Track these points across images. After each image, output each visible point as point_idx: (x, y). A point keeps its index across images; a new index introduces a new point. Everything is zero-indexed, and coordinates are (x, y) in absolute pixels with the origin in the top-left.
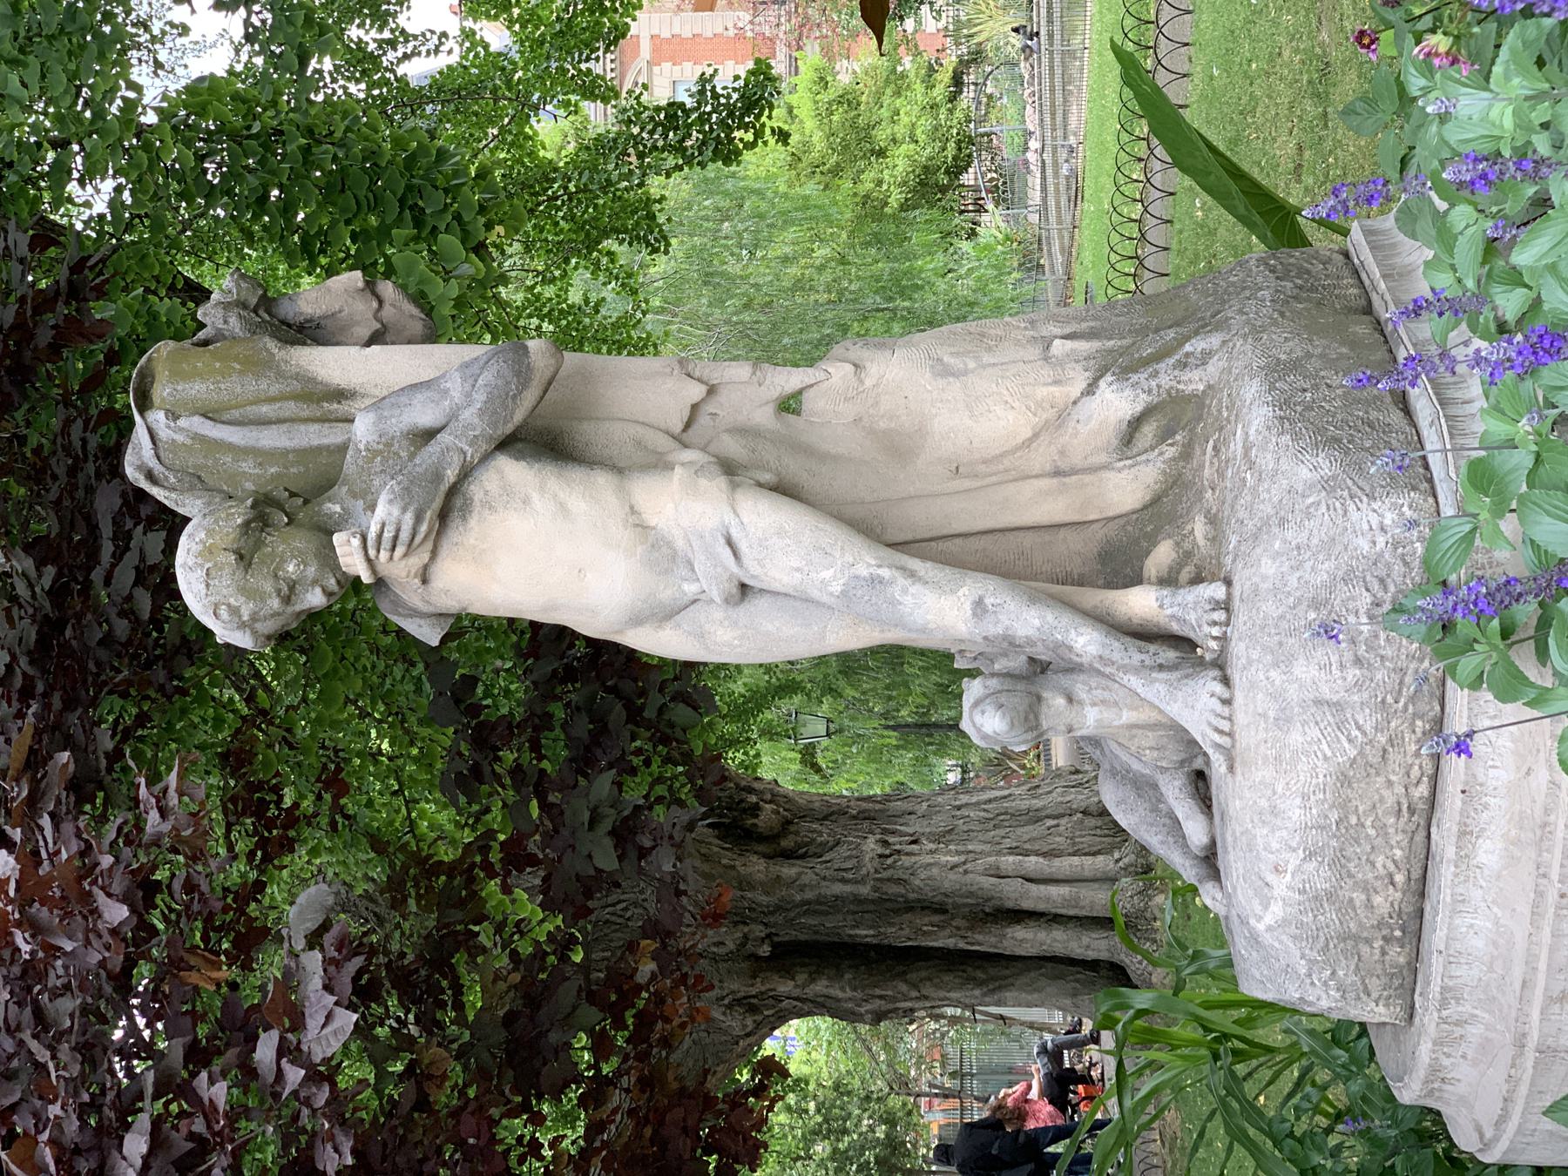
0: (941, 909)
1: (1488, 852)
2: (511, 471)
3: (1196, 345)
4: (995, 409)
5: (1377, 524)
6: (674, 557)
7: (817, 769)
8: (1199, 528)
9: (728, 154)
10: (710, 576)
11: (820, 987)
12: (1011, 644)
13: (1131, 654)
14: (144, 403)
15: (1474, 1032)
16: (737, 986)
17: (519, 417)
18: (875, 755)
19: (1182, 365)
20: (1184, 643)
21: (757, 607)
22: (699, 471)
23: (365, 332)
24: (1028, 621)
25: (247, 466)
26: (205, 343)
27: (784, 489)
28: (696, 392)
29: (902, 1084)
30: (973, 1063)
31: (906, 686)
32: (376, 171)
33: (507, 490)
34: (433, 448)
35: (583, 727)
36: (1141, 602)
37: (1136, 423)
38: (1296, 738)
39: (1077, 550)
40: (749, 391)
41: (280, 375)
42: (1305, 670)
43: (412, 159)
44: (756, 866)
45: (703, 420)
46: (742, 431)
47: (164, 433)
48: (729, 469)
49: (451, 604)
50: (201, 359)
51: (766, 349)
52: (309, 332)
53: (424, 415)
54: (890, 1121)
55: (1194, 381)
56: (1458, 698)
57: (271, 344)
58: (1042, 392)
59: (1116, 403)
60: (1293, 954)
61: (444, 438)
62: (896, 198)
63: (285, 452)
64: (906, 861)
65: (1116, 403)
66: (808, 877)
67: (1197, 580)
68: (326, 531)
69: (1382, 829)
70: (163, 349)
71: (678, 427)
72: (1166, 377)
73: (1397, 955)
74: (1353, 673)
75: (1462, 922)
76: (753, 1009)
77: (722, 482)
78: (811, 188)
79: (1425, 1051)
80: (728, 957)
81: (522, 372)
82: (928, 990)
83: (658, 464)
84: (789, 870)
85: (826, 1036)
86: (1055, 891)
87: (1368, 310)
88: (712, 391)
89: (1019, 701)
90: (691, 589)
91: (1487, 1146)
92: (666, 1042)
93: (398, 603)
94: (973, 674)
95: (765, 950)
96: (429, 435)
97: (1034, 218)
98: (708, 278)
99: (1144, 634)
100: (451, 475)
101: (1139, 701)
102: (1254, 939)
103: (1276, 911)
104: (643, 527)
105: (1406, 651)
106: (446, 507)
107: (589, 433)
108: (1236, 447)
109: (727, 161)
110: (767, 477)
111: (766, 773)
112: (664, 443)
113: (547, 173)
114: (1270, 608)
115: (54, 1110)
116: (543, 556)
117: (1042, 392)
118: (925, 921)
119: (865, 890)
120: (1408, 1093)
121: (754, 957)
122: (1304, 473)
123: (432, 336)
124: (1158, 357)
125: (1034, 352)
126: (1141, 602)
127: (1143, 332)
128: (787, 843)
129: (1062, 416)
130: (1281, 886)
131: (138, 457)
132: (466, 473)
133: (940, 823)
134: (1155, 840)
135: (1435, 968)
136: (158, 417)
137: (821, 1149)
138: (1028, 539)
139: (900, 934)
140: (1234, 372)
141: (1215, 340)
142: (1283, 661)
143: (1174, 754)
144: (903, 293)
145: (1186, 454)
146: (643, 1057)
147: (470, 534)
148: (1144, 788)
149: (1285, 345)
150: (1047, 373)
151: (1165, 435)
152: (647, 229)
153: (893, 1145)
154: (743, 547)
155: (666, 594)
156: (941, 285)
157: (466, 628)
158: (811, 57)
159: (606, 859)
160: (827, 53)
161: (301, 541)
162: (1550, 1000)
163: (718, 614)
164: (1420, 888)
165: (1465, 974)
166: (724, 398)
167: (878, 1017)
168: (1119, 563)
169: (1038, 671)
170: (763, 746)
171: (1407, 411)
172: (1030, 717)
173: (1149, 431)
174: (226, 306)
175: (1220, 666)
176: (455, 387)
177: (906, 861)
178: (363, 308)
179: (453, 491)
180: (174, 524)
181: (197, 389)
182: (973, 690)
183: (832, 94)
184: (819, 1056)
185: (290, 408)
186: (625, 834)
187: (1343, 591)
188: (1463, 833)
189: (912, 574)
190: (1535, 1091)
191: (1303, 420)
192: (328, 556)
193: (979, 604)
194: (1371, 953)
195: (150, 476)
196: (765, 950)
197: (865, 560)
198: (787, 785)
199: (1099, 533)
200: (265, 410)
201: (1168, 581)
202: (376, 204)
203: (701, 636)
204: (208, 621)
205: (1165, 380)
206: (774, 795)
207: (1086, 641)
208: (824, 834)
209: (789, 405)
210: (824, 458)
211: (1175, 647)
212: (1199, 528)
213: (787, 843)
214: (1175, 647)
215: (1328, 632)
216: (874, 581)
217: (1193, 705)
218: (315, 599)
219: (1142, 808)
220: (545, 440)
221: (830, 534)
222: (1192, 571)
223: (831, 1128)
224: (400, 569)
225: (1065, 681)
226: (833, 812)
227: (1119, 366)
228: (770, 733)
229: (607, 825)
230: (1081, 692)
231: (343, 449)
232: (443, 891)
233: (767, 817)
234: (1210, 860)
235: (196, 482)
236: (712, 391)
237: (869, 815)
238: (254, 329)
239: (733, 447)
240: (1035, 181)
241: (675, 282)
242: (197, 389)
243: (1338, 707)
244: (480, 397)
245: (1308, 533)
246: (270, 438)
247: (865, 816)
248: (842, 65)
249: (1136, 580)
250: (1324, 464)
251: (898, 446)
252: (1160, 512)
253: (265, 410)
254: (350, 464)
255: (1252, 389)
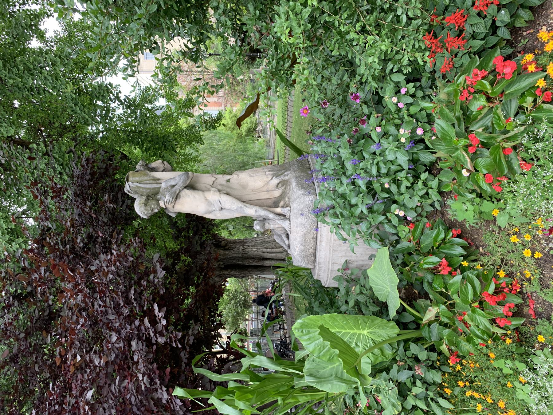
0: (253, 258)
1: (324, 244)
2: (186, 191)
3: (286, 173)
4: (258, 182)
5: (309, 200)
6: (211, 204)
7: (232, 235)
8: (287, 199)
9: (214, 128)
10: (217, 206)
11: (232, 272)
12: (260, 216)
13: (278, 217)
14: (128, 181)
15: (323, 268)
16: (218, 273)
17: (188, 183)
18: (242, 232)
19: (285, 176)
20: (284, 216)
21: (224, 211)
22: (215, 191)
23: (162, 169)
24: (263, 213)
25: (144, 190)
26: (137, 171)
27: (228, 194)
28: (214, 179)
29: (247, 290)
30: (259, 286)
31: (246, 223)
32: (158, 139)
33: (186, 194)
34: (175, 188)
35: (195, 229)
36: (279, 210)
37: (278, 184)
38: (299, 229)
39: (270, 202)
40: (222, 179)
41: (150, 176)
42: (300, 220)
43: (164, 137)
44: (221, 252)
45: (215, 183)
46: (221, 185)
47: (131, 185)
48: (219, 191)
49: (178, 211)
50: (137, 174)
51: (224, 173)
52: (153, 170)
53: (173, 183)
54: (245, 296)
55: (286, 178)
56: (319, 223)
57: (148, 172)
58: (265, 179)
59: (275, 181)
60: (299, 259)
61: (176, 186)
62: (244, 133)
63: (150, 188)
64: (247, 250)
65: (275, 181)
66: (230, 253)
67: (287, 207)
68: (158, 201)
69: (310, 241)
70: (131, 172)
71: (211, 184)
72: (282, 177)
73: (313, 258)
74: (306, 220)
75: (321, 253)
76: (221, 277)
77: (218, 193)
78: (229, 132)
79: (317, 271)
80: (217, 268)
81: (188, 177)
82: (251, 272)
83: (209, 190)
84: (227, 252)
85: (233, 282)
86: (273, 255)
87: (310, 168)
88: (216, 179)
89: (262, 224)
90: (214, 208)
91: (326, 284)
92: (209, 278)
93: (169, 211)
94: (255, 220)
95: (223, 266)
96: (174, 186)
97: (269, 137)
98: (211, 148)
99: (279, 215)
100: (177, 192)
101: (279, 224)
102: (294, 257)
103: (297, 252)
104: (207, 200)
105: (313, 217)
106: (177, 197)
107: (198, 185)
108: (291, 188)
109: (214, 129)
110: (225, 192)
111: (222, 235)
112: (209, 187)
113: (182, 131)
114: (295, 211)
115: (120, 287)
116: (192, 204)
117: (265, 179)
118: (250, 260)
119: (240, 255)
120: (315, 278)
121: (221, 268)
122: (300, 192)
123: (173, 170)
124: (281, 175)
125: (264, 173)
126: (279, 210)
127: (279, 170)
128: (226, 248)
129: (268, 183)
130: (297, 249)
131: (127, 189)
132: (180, 192)
133: (253, 243)
134: (282, 244)
135: (317, 259)
136: (130, 183)
137: (233, 302)
138: (263, 201)
139: (246, 263)
140: (290, 176)
141: (289, 172)
142: (297, 218)
143: (284, 231)
144: (246, 151)
145: (285, 188)
146: (205, 281)
147: (180, 201)
148: (280, 236)
149: (298, 173)
150: (265, 177)
151: (282, 186)
152: (200, 140)
153: (245, 300)
154: (222, 202)
155: (210, 209)
156: (252, 150)
157: (179, 214)
158: (228, 108)
159: (199, 249)
160: (232, 107)
161: (154, 202)
162: (332, 263)
163: (218, 212)
164: (316, 249)
165: (322, 260)
166: (218, 180)
167: (243, 277)
168: (276, 204)
169: (265, 220)
170: (222, 231)
171: (314, 184)
172: (263, 226)
173: (280, 185)
174: (140, 166)
175: (289, 219)
176: (178, 179)
177: (247, 250)
178: (162, 166)
179: (178, 194)
180: (133, 200)
181: (136, 179)
182: (255, 222)
183: (232, 115)
184: (232, 286)
185: (151, 181)
186: (202, 245)
187: (305, 209)
188: (320, 241)
189: (246, 206)
190: (331, 276)
191: (300, 185)
192: (158, 204)
193: (256, 210)
194: (309, 258)
195: (129, 192)
196: (223, 266)
197: (239, 204)
198: (226, 237)
199: (273, 200)
200: (147, 182)
201: (283, 207)
202: (158, 143)
203: (215, 215)
204: (140, 214)
205: (282, 178)
206: (224, 239)
207: (271, 216)
208: (233, 246)
209: (228, 181)
210: (233, 189)
211: (283, 216)
212: (287, 199)
213: (226, 248)
214: (283, 216)
215: (302, 215)
216: (241, 207)
217: (285, 224)
218: (156, 211)
219: (280, 239)
220: (191, 187)
221: (235, 201)
222: (287, 205)
223: (234, 297)
224: (169, 206)
225: (268, 221)
226: (235, 242)
227: (276, 176)
228: (223, 228)
229: (199, 244)
230: (270, 223)
231: (160, 188)
232: (175, 256)
233: (223, 243)
234: (289, 246)
235: (136, 193)
236: (216, 179)
237: (241, 242)
238: (145, 169)
239: (220, 187)
240: (269, 130)
241: (205, 149)
242: (136, 179)
243: (304, 224)
244: (182, 181)
245: (300, 201)
246: (148, 186)
247: (240, 243)
248: (234, 108)
249: (278, 207)
250: (303, 191)
251: (244, 187)
252: (282, 197)
253: (147, 182)
254: (161, 190)
255: (293, 180)
